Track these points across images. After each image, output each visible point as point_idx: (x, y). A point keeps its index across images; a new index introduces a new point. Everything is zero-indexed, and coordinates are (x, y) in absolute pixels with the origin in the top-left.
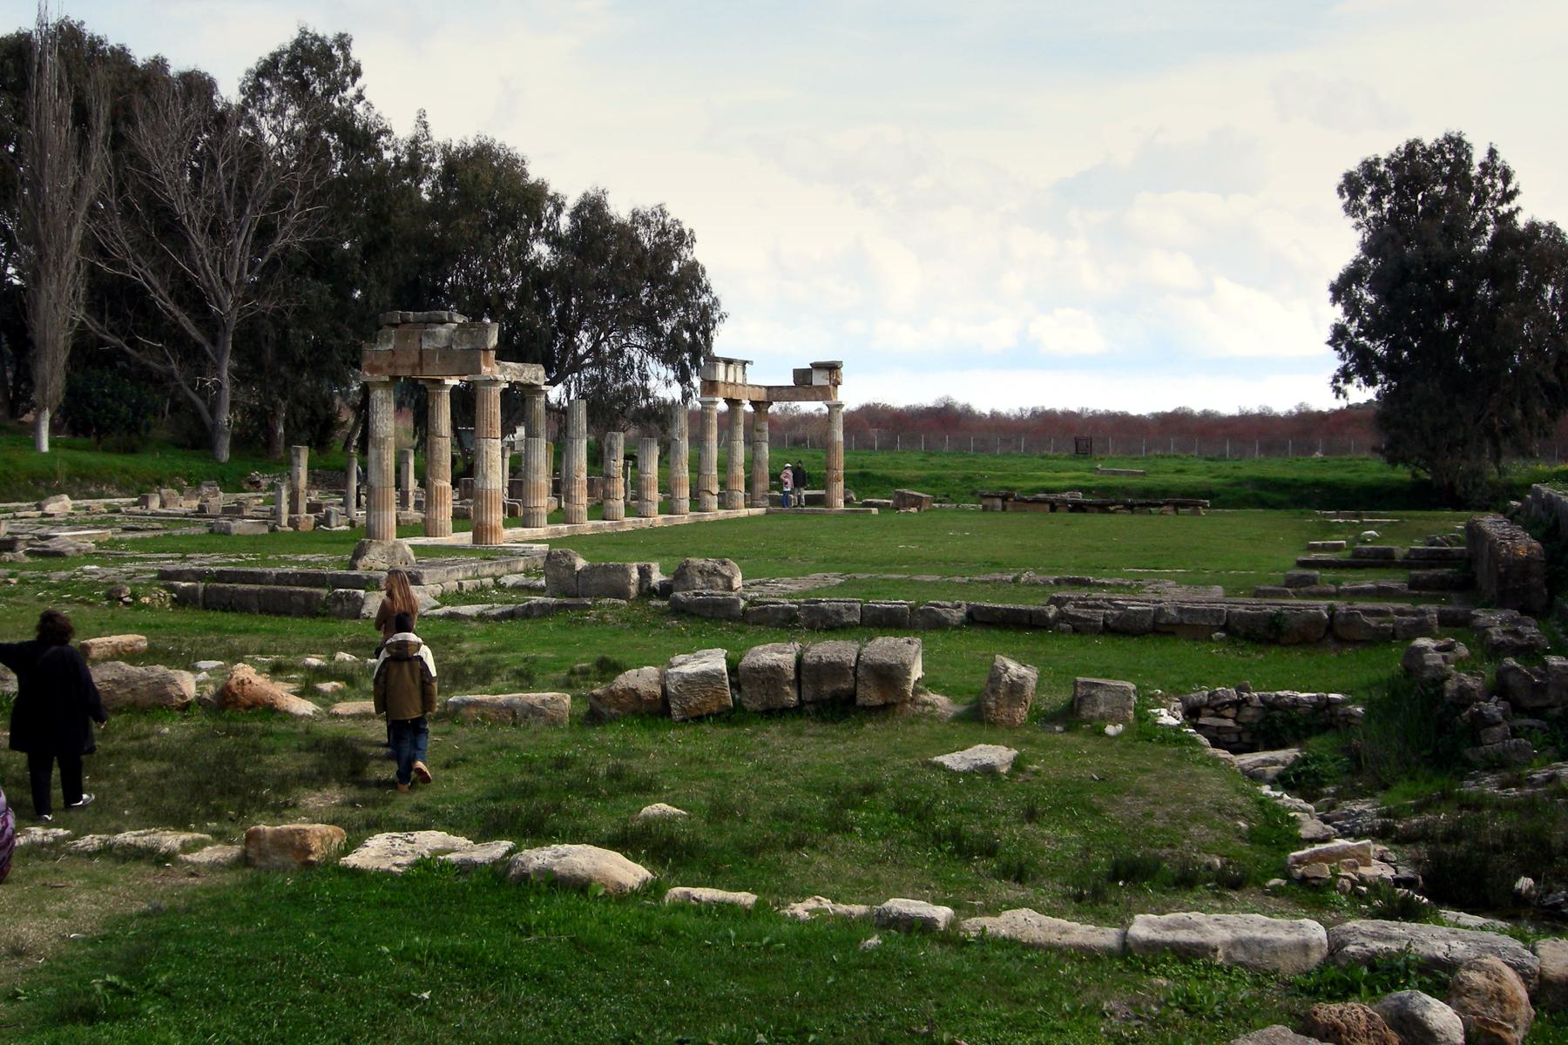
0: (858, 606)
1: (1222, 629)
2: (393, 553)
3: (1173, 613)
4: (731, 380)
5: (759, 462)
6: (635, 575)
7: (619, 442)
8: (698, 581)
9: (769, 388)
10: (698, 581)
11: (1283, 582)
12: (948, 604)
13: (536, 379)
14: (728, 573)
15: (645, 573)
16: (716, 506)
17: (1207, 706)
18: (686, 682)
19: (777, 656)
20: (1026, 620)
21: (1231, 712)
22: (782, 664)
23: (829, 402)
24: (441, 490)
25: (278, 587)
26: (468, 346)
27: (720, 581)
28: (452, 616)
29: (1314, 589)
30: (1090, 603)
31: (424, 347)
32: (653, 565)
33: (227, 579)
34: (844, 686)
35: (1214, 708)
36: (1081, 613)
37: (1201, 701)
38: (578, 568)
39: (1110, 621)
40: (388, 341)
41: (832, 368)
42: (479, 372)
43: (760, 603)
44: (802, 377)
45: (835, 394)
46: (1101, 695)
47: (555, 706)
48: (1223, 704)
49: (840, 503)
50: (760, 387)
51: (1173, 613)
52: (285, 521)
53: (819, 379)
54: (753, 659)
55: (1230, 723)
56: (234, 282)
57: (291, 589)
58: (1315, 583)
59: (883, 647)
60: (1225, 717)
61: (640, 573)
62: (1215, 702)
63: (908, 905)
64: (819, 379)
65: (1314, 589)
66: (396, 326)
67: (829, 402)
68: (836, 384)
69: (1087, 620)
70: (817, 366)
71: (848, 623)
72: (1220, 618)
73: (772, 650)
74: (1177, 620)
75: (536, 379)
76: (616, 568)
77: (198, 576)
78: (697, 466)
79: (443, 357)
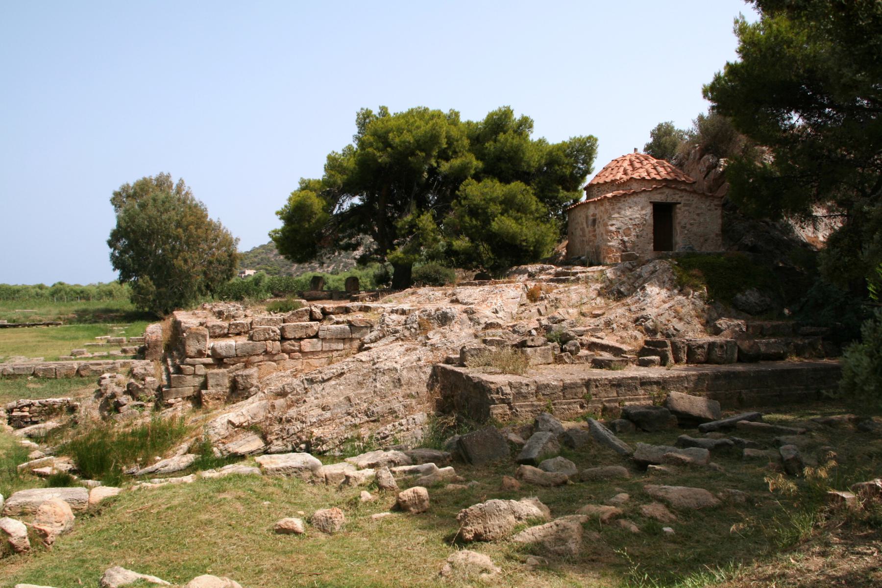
11: (70, 354)
17: (16, 408)
21: (27, 409)
29: (83, 356)
51: (11, 370)
55: (27, 414)
65: (83, 356)
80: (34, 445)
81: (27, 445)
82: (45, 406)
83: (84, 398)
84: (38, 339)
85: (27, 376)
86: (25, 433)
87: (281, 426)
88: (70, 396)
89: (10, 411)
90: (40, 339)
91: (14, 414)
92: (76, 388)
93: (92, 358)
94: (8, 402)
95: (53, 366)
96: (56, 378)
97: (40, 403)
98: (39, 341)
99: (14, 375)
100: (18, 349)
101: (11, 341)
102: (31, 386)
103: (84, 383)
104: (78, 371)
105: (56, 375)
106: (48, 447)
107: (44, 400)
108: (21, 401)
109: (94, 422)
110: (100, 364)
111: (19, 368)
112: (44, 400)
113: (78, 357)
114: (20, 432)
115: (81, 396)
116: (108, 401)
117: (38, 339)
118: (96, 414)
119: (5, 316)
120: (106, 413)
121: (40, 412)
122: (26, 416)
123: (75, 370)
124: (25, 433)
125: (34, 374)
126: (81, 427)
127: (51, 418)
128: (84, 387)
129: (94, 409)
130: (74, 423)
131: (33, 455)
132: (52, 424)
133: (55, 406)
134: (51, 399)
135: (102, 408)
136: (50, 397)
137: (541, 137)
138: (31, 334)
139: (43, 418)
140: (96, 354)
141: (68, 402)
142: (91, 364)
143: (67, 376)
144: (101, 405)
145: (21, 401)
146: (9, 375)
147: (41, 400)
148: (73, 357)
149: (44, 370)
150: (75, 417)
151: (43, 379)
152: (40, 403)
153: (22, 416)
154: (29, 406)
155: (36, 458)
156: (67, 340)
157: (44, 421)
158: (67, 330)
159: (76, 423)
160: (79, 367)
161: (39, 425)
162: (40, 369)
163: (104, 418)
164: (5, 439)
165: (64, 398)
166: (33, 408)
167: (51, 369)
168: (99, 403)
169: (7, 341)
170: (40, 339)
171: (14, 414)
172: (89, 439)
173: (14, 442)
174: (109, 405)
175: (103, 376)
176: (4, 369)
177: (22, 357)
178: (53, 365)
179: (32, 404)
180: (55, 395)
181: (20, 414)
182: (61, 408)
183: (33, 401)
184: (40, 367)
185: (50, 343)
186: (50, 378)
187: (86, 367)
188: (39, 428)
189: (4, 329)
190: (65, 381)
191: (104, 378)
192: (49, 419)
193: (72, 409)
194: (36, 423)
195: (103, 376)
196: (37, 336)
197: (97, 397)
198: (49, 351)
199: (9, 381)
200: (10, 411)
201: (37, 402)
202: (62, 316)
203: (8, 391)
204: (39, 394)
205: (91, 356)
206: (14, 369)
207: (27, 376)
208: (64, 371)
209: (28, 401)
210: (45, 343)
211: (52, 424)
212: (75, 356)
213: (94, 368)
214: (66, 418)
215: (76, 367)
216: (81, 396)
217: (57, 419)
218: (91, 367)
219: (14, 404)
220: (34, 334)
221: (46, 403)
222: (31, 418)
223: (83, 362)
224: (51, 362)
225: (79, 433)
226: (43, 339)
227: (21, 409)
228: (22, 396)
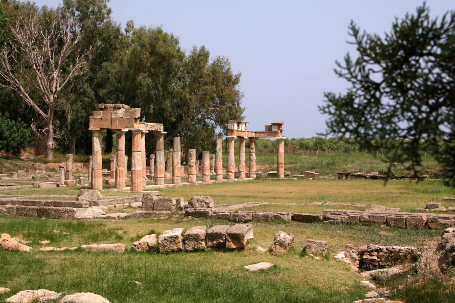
0: (251, 214)
1: (385, 223)
2: (93, 194)
3: (367, 218)
4: (240, 129)
5: (252, 161)
6: (175, 202)
7: (193, 152)
8: (197, 204)
10: (197, 204)
11: (425, 206)
12: (285, 213)
14: (208, 202)
15: (178, 201)
16: (234, 177)
17: (366, 251)
18: (165, 239)
19: (199, 230)
21: (376, 254)
22: (199, 233)
24: (122, 171)
25: (44, 207)
26: (129, 117)
28: (108, 218)
29: (437, 209)
30: (336, 213)
32: (181, 199)
33: (26, 204)
34: (221, 241)
35: (369, 252)
36: (332, 217)
37: (364, 249)
38: (154, 200)
39: (343, 220)
40: (99, 115)
41: (279, 125)
42: (133, 127)
43: (218, 213)
46: (313, 246)
47: (119, 248)
48: (372, 251)
49: (282, 176)
51: (367, 218)
52: (63, 182)
54: (190, 232)
55: (375, 258)
56: (54, 90)
57: (49, 207)
58: (438, 207)
59: (237, 228)
60: (373, 256)
61: (177, 201)
62: (369, 250)
64: (274, 129)
65: (437, 209)
70: (274, 124)
71: (248, 220)
72: (384, 219)
73: (198, 228)
74: (368, 220)
76: (167, 200)
77: (13, 203)
78: (238, 161)
80: (372, 285)
81: (366, 285)
82: (391, 252)
83: (427, 249)
84: (401, 191)
85: (379, 223)
86: (371, 275)
87: (72, 228)
88: (414, 246)
89: (361, 254)
90: (403, 191)
91: (365, 257)
92: (422, 239)
93: (445, 212)
94: (361, 246)
95: (404, 217)
96: (406, 228)
97: (387, 249)
98: (402, 193)
99: (369, 221)
100: (380, 200)
101: (378, 191)
102: (383, 233)
103: (431, 235)
104: (426, 223)
105: (406, 225)
106: (387, 290)
107: (391, 247)
108: (371, 245)
109: (432, 273)
110: (448, 218)
111: (373, 216)
112: (391, 247)
113: (432, 210)
114: (366, 274)
115: (425, 247)
116: (447, 254)
117: (401, 191)
118: (435, 266)
119: (378, 168)
120: (444, 266)
121: (387, 258)
122: (375, 260)
123: (424, 223)
124: (371, 275)
125: (386, 223)
126: (420, 277)
127: (397, 264)
128: (431, 239)
129: (433, 260)
130: (415, 271)
131: (369, 294)
132: (395, 270)
133: (401, 254)
134: (397, 247)
135: (441, 261)
136: (396, 245)
137: (143, 26)
138: (397, 186)
139: (389, 263)
140: (451, 208)
141: (412, 251)
142: (440, 218)
143: (416, 227)
144: (441, 257)
145: (371, 245)
146: (365, 221)
147: (388, 247)
148: (427, 210)
149: (396, 220)
150: (416, 266)
151: (394, 227)
152: (387, 249)
153: (371, 259)
154: (378, 251)
155: (371, 298)
156: (428, 193)
157: (390, 266)
158: (431, 183)
159: (416, 271)
160: (428, 219)
161: (385, 270)
162: (392, 219)
163: (442, 270)
164: (349, 277)
165: (409, 247)
166: (382, 253)
167: (402, 219)
168: (440, 255)
169: (374, 191)
170: (403, 191)
171: (365, 257)
172: (423, 288)
173: (355, 281)
174: (448, 258)
175: (447, 229)
176: (361, 216)
177: (382, 207)
178: (404, 215)
179: (380, 249)
180: (402, 243)
181: (369, 257)
182: (405, 256)
183: (381, 247)
184: (392, 216)
185: (412, 195)
186: (401, 228)
187: (434, 220)
188: (383, 272)
189: (375, 180)
190: (414, 232)
191: (448, 232)
192: (395, 265)
193: (415, 258)
194: (383, 267)
195: (447, 229)
196: (402, 188)
197: (438, 249)
198: (408, 203)
199: (365, 227)
200: (361, 254)
201: (384, 248)
202: (429, 170)
203: (362, 236)
204: (388, 241)
205: (445, 210)
206: (369, 217)
207: (379, 223)
208: (413, 222)
209: (377, 247)
210: (406, 195)
211: (395, 270)
212: (430, 209)
213: (443, 221)
214: (408, 266)
215: (425, 219)
216: (425, 247)
217: (401, 266)
218: (439, 220)
219: (364, 247)
220: (400, 186)
221: (392, 250)
222: (379, 262)
223: (432, 215)
224: (403, 213)
225: (417, 281)
226: (407, 191)
227: (370, 253)
228: (373, 241)
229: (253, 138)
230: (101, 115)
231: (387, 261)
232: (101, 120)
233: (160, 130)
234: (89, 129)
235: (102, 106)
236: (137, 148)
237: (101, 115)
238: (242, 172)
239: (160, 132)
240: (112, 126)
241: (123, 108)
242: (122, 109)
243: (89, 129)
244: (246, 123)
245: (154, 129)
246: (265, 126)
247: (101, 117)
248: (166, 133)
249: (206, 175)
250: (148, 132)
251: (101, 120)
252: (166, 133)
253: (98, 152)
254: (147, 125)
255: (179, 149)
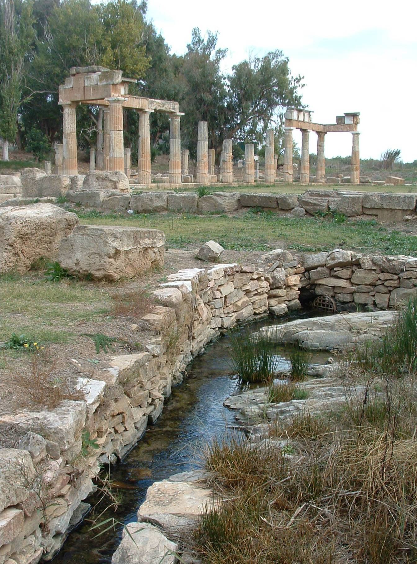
9: (324, 125)
13: (174, 109)
20: (274, 205)
23: (353, 132)
27: (109, 184)
31: (86, 85)
40: (70, 83)
41: (354, 116)
44: (340, 119)
45: (356, 128)
49: (357, 181)
50: (320, 125)
51: (377, 199)
53: (348, 121)
55: (342, 283)
63: (324, 320)
64: (348, 121)
66: (74, 75)
67: (353, 132)
68: (357, 124)
69: (315, 205)
70: (347, 115)
75: (174, 109)
79: (94, 90)
166: (359, 274)
209: (348, 254)
221: (386, 265)
229: (321, 132)
230: (72, 83)
231: (373, 293)
232: (72, 89)
233: (173, 111)
234: (59, 103)
235: (73, 70)
236: (116, 126)
237: (72, 83)
238: (304, 175)
239: (175, 113)
240: (84, 96)
241: (99, 71)
242: (97, 73)
243: (59, 103)
244: (310, 112)
245: (164, 109)
246: (337, 117)
247: (72, 86)
248: (183, 114)
249: (248, 174)
250: (153, 111)
251: (72, 89)
252: (183, 114)
253: (69, 135)
254: (153, 102)
255: (205, 138)
